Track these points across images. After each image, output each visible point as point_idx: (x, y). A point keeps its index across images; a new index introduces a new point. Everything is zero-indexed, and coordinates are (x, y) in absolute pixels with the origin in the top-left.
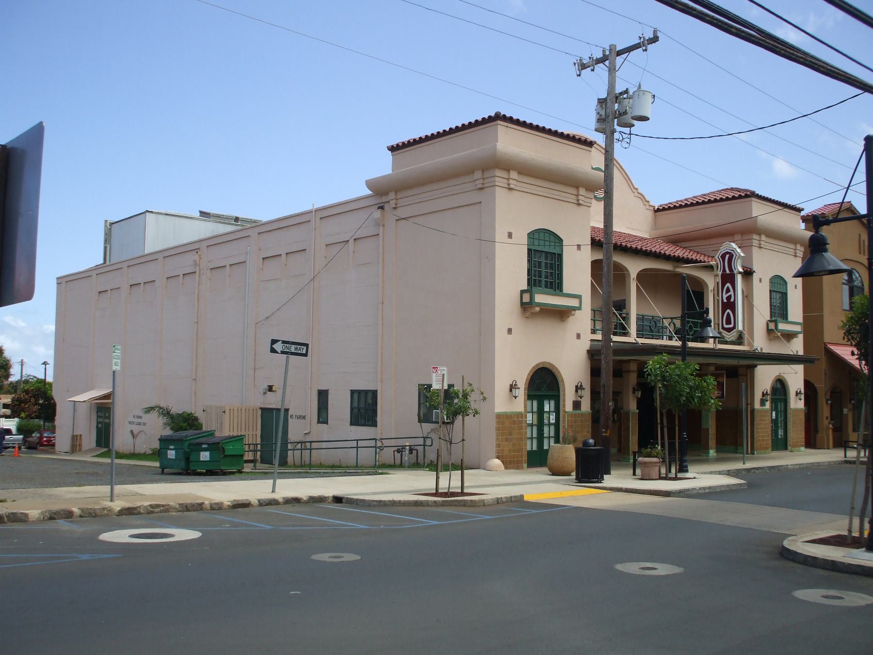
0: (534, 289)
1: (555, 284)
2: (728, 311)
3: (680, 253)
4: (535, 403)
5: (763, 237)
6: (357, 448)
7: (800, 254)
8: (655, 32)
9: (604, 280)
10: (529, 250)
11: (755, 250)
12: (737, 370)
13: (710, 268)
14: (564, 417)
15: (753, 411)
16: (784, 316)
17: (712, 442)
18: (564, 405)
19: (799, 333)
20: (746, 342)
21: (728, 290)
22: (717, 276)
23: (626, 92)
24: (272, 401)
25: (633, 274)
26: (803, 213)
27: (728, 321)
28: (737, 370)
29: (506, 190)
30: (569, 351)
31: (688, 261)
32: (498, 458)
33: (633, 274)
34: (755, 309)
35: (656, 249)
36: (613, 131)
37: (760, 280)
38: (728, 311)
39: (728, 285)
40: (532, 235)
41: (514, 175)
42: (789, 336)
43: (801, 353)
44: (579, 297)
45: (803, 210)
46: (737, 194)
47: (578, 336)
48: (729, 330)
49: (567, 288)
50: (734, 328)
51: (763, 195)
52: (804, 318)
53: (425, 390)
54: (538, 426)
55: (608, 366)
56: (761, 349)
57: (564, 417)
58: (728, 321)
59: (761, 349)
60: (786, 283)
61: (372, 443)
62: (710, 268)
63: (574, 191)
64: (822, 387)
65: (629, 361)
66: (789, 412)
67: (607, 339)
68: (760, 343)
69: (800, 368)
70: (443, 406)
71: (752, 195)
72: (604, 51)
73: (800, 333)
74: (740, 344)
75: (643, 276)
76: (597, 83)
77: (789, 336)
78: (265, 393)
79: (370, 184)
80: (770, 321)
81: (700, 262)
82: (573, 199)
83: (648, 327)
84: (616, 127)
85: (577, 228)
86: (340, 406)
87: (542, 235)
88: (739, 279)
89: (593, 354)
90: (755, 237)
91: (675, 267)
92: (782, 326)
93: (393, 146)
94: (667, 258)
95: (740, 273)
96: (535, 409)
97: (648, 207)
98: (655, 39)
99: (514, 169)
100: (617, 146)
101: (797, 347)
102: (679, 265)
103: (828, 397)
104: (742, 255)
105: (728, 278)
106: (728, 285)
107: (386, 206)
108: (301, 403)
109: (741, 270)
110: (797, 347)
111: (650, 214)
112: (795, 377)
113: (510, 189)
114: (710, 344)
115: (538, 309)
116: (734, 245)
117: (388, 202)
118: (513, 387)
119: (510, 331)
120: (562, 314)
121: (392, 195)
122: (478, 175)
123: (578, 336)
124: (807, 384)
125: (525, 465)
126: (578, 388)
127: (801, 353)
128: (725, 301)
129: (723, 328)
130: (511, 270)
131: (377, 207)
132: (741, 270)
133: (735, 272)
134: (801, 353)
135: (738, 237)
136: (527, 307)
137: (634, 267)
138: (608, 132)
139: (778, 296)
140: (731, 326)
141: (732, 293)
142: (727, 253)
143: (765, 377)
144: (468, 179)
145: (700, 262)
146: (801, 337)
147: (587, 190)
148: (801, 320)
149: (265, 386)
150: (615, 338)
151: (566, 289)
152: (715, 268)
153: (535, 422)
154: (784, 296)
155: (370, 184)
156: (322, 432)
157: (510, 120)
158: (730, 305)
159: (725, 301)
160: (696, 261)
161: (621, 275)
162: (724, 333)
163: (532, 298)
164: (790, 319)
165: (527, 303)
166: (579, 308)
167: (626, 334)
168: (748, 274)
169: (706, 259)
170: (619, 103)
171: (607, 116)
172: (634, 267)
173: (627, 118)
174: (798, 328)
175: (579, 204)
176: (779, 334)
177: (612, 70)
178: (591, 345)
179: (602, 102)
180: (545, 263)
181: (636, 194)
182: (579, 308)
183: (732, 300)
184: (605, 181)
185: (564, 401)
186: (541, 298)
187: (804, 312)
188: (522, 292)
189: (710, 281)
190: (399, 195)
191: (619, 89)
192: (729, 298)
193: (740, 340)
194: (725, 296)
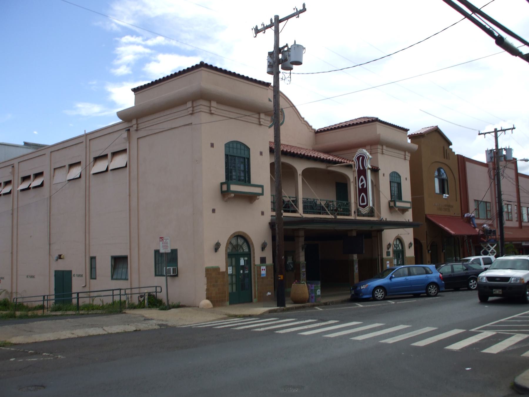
0: (230, 181)
1: (246, 180)
2: (363, 194)
3: (331, 158)
4: (234, 260)
5: (384, 147)
6: (113, 295)
7: (408, 158)
8: (304, 5)
9: (275, 173)
10: (227, 156)
11: (380, 156)
12: (371, 233)
13: (350, 166)
14: (254, 268)
15: (382, 259)
16: (400, 198)
17: (303, 277)
18: (254, 261)
19: (409, 208)
20: (376, 214)
21: (362, 181)
22: (354, 171)
23: (287, 46)
24: (62, 266)
25: (300, 172)
26: (409, 133)
27: (363, 201)
28: (371, 233)
29: (209, 115)
30: (256, 222)
31: (335, 162)
32: (208, 298)
33: (300, 172)
34: (381, 194)
35: (316, 154)
36: (278, 72)
37: (384, 175)
38: (363, 194)
39: (362, 177)
40: (228, 145)
41: (214, 104)
42: (403, 210)
43: (411, 220)
44: (262, 187)
45: (409, 130)
46: (366, 120)
47: (263, 213)
48: (364, 207)
49: (254, 180)
50: (367, 205)
51: (383, 120)
52: (412, 198)
53: (157, 252)
54: (236, 275)
55: (283, 233)
56: (386, 219)
57: (254, 268)
58: (363, 201)
59: (386, 219)
60: (400, 177)
61: (111, 293)
62: (350, 166)
63: (257, 116)
64: (424, 242)
65: (298, 230)
66: (405, 259)
67: (279, 214)
68: (385, 215)
69: (411, 230)
70: (167, 262)
71: (376, 120)
72: (271, 20)
73: (409, 208)
74: (372, 216)
75: (306, 173)
76: (266, 42)
77: (403, 210)
78: (57, 260)
79: (120, 115)
80: (391, 201)
81: (344, 163)
82: (256, 121)
83: (310, 206)
84: (280, 69)
85: (258, 141)
86: (104, 266)
87: (239, 145)
88: (369, 173)
89: (272, 225)
90: (379, 147)
91: (328, 167)
92: (398, 204)
93: (134, 89)
94: (322, 161)
95: (369, 169)
96: (234, 264)
97: (311, 130)
98: (304, 10)
99: (214, 100)
100: (281, 83)
101: (408, 217)
102: (330, 165)
103: (429, 248)
104: (370, 157)
105: (362, 172)
106: (362, 177)
107: (131, 129)
108: (76, 265)
109: (370, 167)
110: (408, 217)
111: (312, 134)
112: (408, 236)
113: (212, 114)
114: (352, 217)
115: (233, 195)
116: (365, 151)
117: (132, 126)
118: (217, 247)
119: (214, 211)
120: (251, 198)
121: (134, 122)
122: (189, 104)
123: (263, 213)
124: (416, 241)
125: (228, 303)
126: (263, 247)
127: (411, 220)
128: (360, 187)
129: (360, 205)
130: (215, 170)
131: (125, 130)
132: (370, 167)
133: (366, 168)
134: (411, 220)
135: (368, 147)
136: (225, 194)
137: (300, 167)
138: (274, 73)
139: (396, 185)
140: (365, 204)
141: (364, 182)
142: (360, 156)
143: (389, 236)
144: (183, 107)
145: (344, 163)
146: (410, 211)
147: (265, 115)
148: (410, 200)
149: (57, 255)
150: (285, 214)
151: (253, 182)
152: (353, 166)
153: (234, 273)
154: (399, 185)
155: (120, 115)
156: (95, 285)
157: (211, 67)
158: (363, 190)
159: (360, 187)
160: (341, 162)
161: (290, 172)
162: (361, 209)
163: (228, 187)
164: (403, 199)
165: (225, 192)
166: (262, 194)
167: (295, 211)
168: (375, 170)
169: (345, 161)
170: (282, 54)
171: (274, 62)
172: (300, 167)
173: (288, 63)
174: (408, 205)
175: (260, 125)
176: (397, 209)
177: (277, 32)
178: (272, 219)
179: (270, 54)
180: (237, 163)
181: (303, 122)
182: (262, 194)
183: (365, 187)
184: (274, 106)
185: (254, 257)
186: (234, 188)
187: (412, 195)
188: (222, 184)
189: (351, 175)
190: (140, 121)
191: (281, 46)
192: (363, 185)
193: (371, 213)
194: (360, 185)
